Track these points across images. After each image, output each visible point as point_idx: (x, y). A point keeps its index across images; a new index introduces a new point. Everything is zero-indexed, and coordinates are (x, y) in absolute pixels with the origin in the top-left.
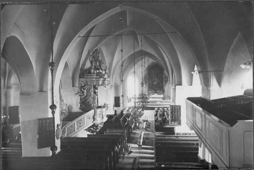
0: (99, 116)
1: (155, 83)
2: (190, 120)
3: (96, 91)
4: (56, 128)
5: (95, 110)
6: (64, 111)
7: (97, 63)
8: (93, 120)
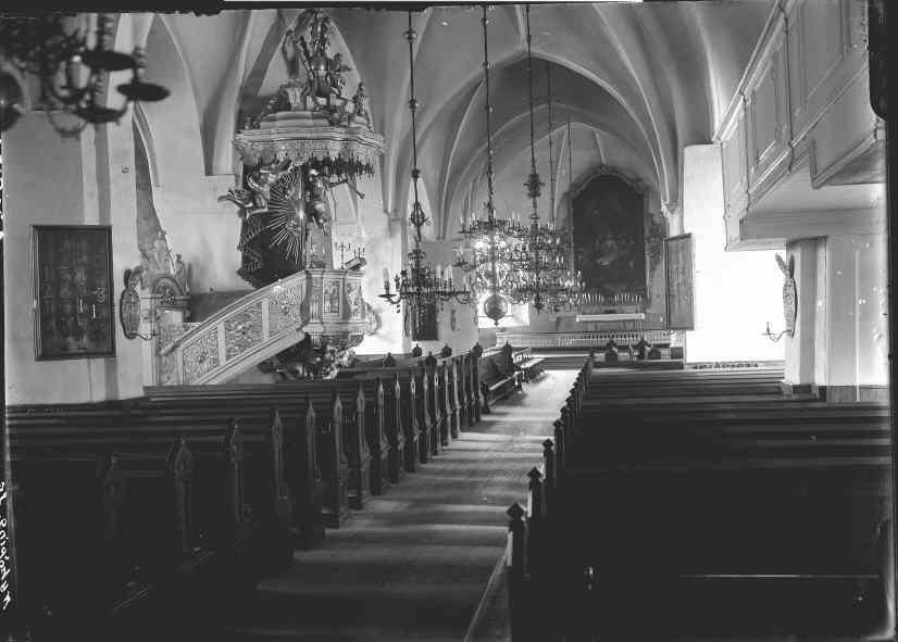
3: (320, 206)
4: (119, 287)
5: (309, 278)
6: (162, 281)
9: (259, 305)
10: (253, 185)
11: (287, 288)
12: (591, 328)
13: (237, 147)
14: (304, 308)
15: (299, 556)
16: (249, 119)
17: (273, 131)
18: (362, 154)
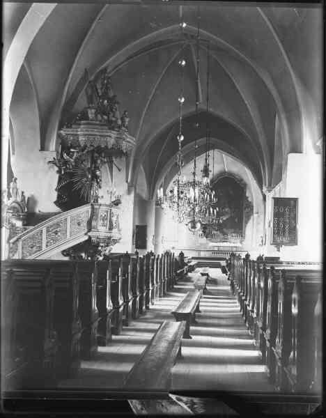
0: (102, 221)
2: (120, 67)
5: (93, 208)
8: (86, 230)
9: (66, 219)
10: (273, 348)
11: (83, 211)
12: (216, 249)
13: (59, 136)
14: (89, 223)
15: (101, 349)
17: (79, 130)
18: (124, 146)
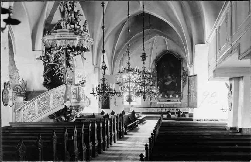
1: (168, 84)
4: (2, 88)
5: (67, 87)
6: (17, 86)
7: (71, 15)
9: (49, 95)
10: (48, 54)
14: (65, 97)
16: (47, 32)
